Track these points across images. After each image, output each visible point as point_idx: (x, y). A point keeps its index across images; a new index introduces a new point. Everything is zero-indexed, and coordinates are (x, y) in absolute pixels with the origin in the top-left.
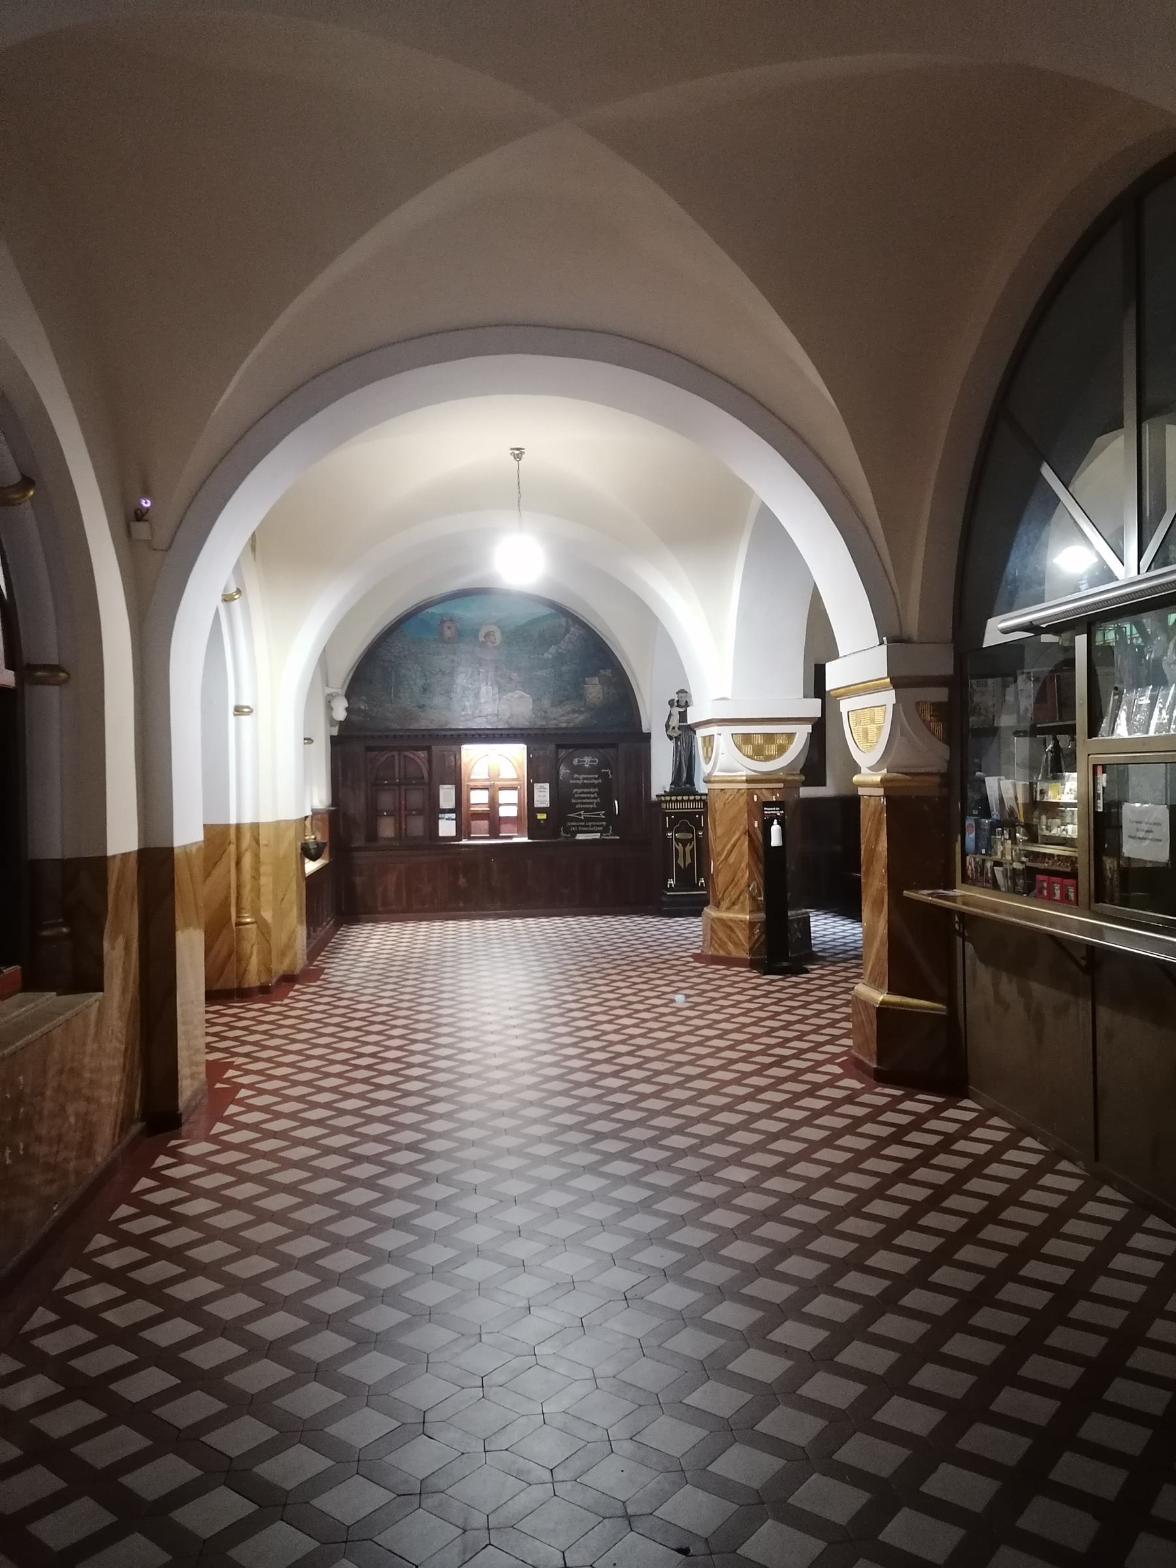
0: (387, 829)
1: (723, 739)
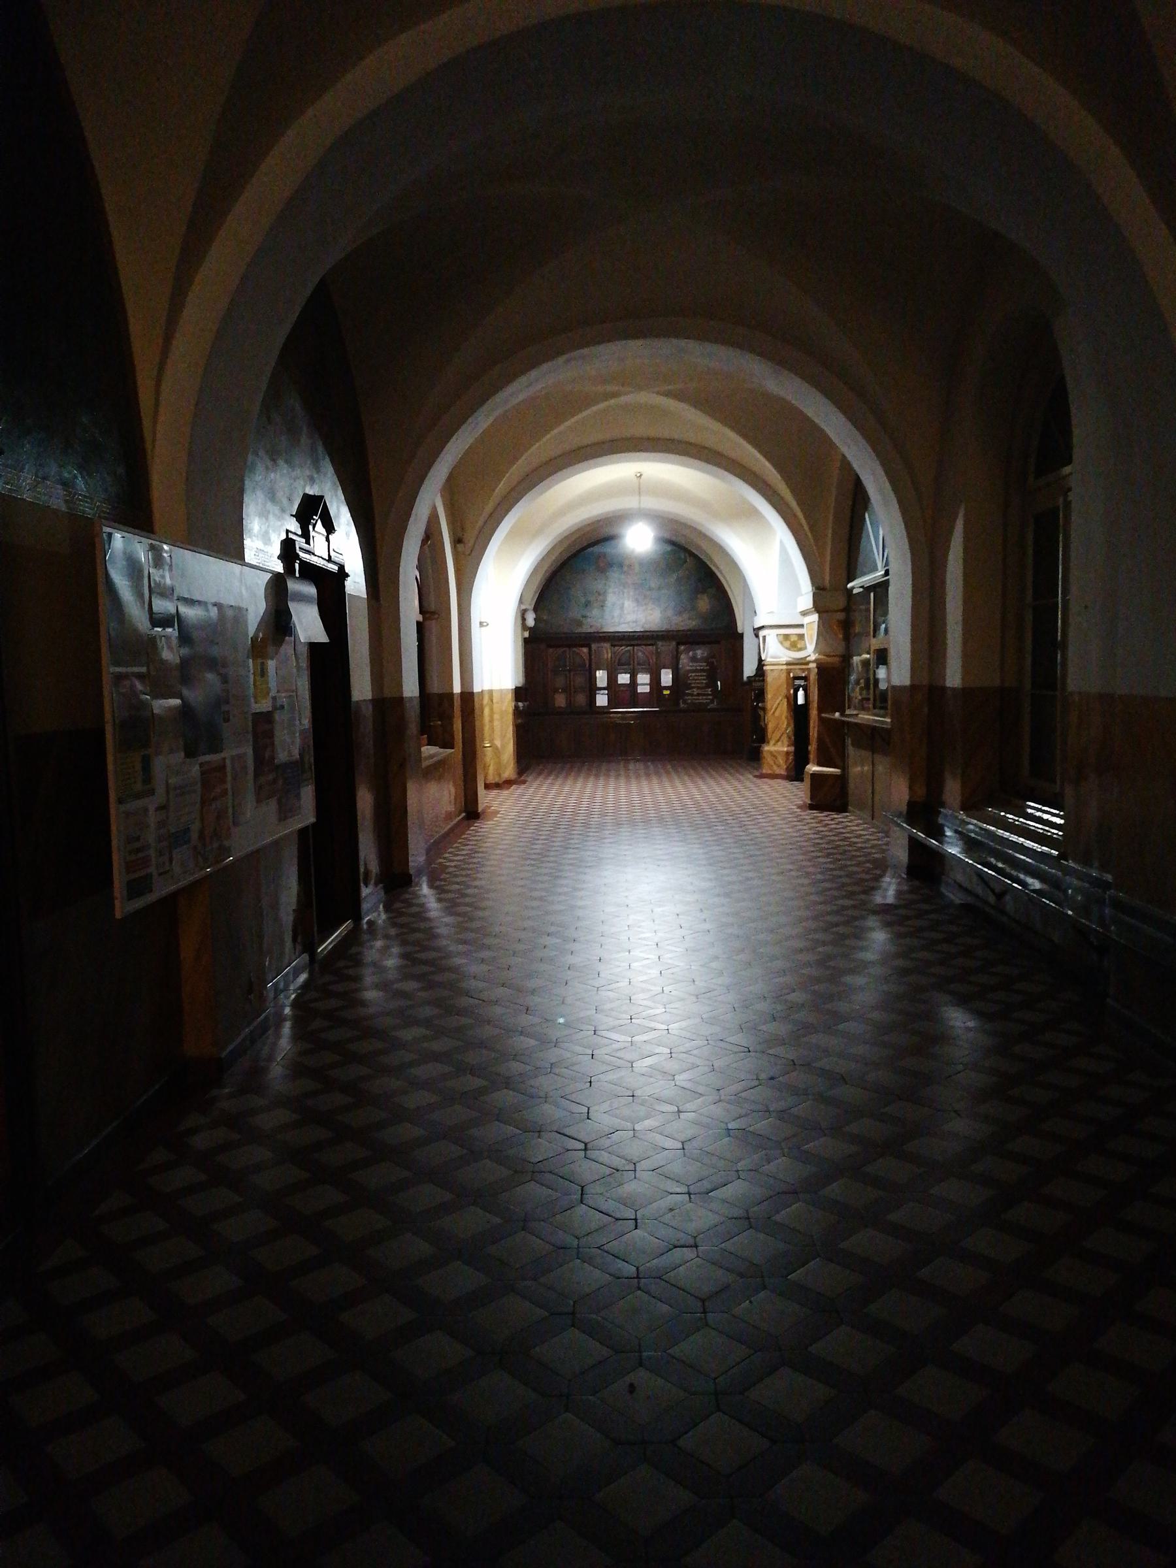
0: (560, 701)
1: (771, 636)
